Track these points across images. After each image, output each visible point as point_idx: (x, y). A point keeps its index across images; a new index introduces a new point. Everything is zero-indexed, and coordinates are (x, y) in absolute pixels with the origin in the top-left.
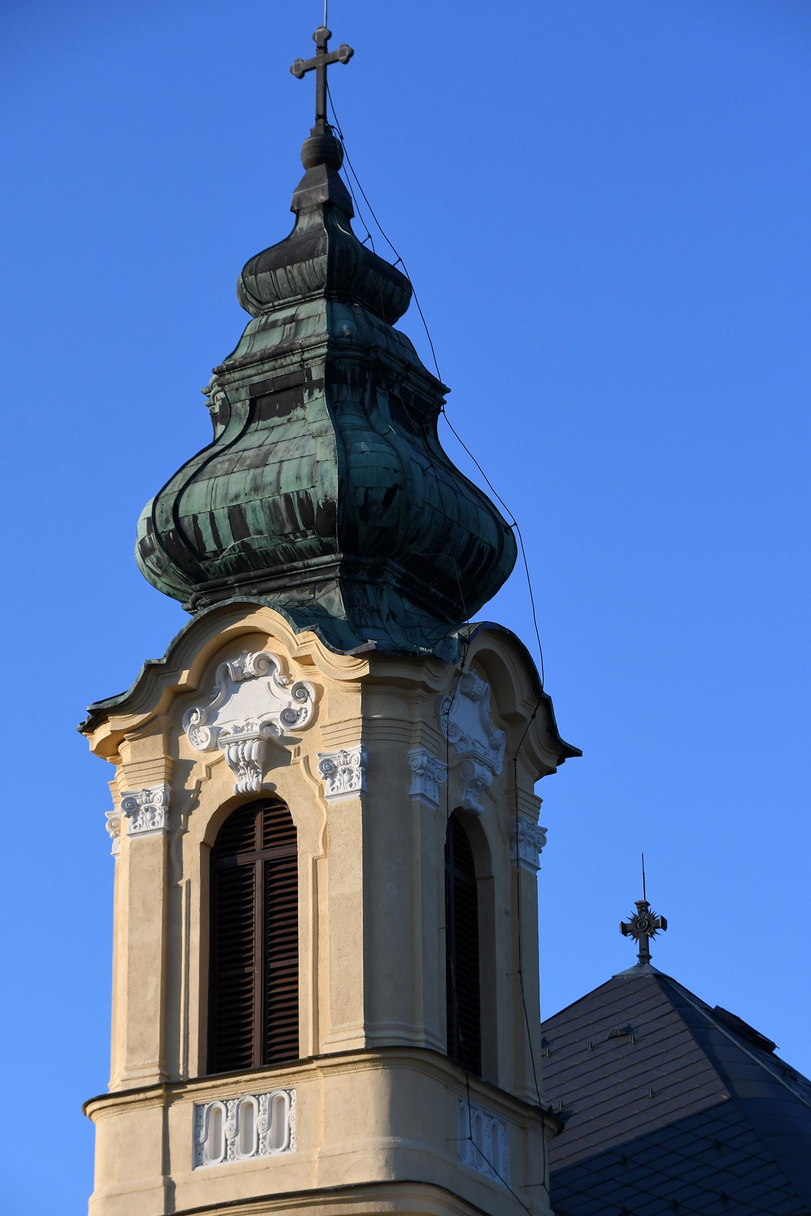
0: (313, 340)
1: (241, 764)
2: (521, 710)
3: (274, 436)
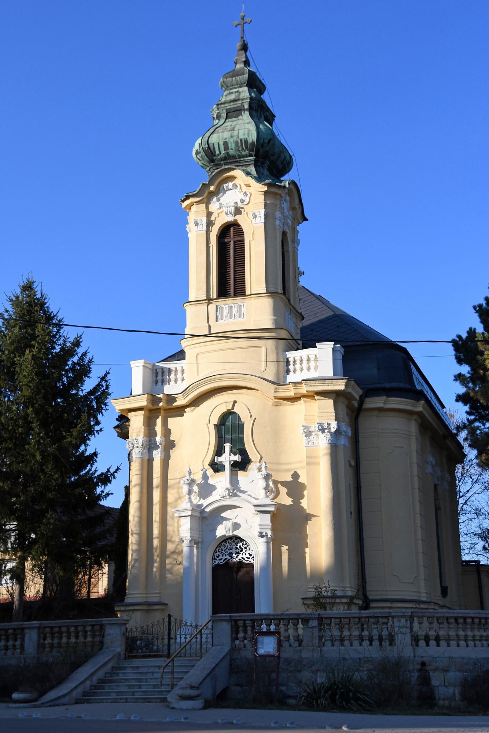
0: (245, 97)
1: (229, 213)
2: (296, 206)
3: (234, 123)
